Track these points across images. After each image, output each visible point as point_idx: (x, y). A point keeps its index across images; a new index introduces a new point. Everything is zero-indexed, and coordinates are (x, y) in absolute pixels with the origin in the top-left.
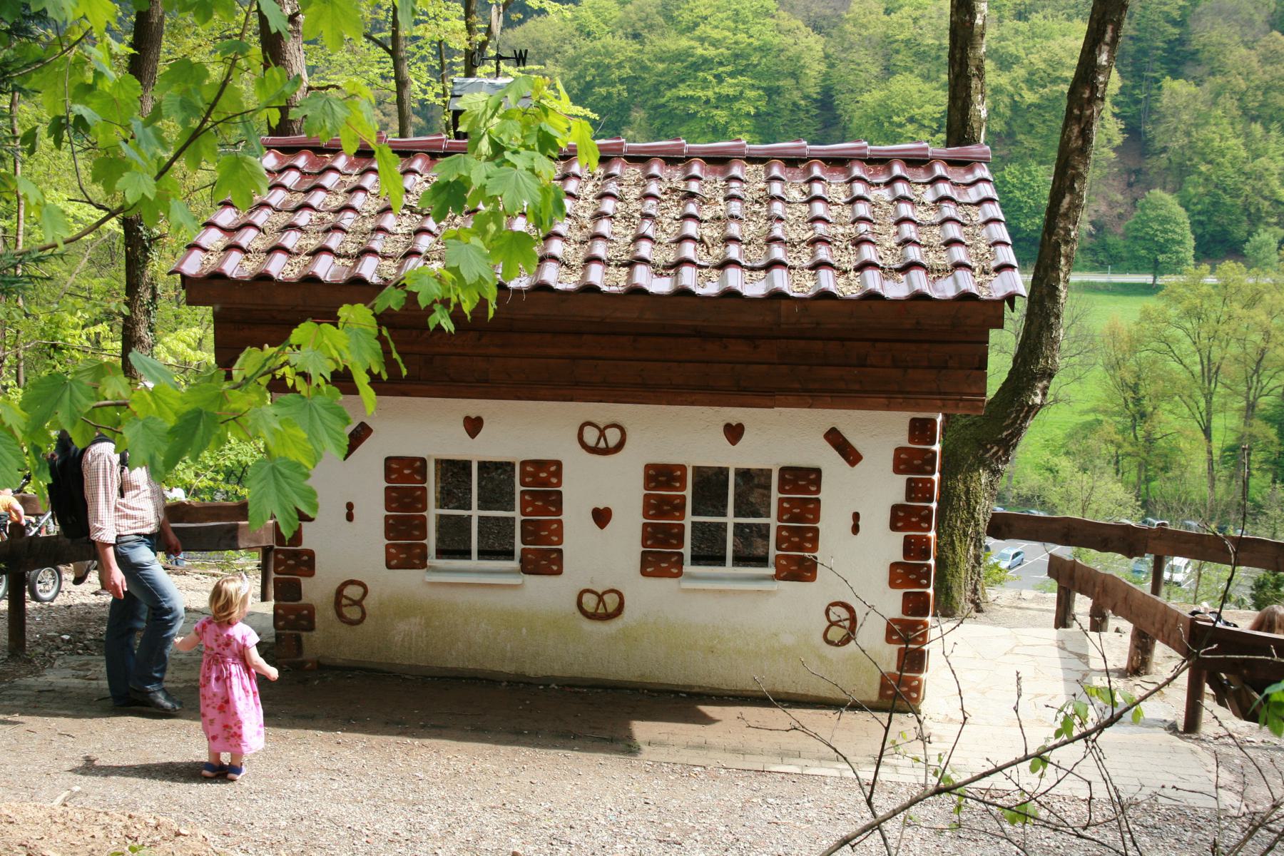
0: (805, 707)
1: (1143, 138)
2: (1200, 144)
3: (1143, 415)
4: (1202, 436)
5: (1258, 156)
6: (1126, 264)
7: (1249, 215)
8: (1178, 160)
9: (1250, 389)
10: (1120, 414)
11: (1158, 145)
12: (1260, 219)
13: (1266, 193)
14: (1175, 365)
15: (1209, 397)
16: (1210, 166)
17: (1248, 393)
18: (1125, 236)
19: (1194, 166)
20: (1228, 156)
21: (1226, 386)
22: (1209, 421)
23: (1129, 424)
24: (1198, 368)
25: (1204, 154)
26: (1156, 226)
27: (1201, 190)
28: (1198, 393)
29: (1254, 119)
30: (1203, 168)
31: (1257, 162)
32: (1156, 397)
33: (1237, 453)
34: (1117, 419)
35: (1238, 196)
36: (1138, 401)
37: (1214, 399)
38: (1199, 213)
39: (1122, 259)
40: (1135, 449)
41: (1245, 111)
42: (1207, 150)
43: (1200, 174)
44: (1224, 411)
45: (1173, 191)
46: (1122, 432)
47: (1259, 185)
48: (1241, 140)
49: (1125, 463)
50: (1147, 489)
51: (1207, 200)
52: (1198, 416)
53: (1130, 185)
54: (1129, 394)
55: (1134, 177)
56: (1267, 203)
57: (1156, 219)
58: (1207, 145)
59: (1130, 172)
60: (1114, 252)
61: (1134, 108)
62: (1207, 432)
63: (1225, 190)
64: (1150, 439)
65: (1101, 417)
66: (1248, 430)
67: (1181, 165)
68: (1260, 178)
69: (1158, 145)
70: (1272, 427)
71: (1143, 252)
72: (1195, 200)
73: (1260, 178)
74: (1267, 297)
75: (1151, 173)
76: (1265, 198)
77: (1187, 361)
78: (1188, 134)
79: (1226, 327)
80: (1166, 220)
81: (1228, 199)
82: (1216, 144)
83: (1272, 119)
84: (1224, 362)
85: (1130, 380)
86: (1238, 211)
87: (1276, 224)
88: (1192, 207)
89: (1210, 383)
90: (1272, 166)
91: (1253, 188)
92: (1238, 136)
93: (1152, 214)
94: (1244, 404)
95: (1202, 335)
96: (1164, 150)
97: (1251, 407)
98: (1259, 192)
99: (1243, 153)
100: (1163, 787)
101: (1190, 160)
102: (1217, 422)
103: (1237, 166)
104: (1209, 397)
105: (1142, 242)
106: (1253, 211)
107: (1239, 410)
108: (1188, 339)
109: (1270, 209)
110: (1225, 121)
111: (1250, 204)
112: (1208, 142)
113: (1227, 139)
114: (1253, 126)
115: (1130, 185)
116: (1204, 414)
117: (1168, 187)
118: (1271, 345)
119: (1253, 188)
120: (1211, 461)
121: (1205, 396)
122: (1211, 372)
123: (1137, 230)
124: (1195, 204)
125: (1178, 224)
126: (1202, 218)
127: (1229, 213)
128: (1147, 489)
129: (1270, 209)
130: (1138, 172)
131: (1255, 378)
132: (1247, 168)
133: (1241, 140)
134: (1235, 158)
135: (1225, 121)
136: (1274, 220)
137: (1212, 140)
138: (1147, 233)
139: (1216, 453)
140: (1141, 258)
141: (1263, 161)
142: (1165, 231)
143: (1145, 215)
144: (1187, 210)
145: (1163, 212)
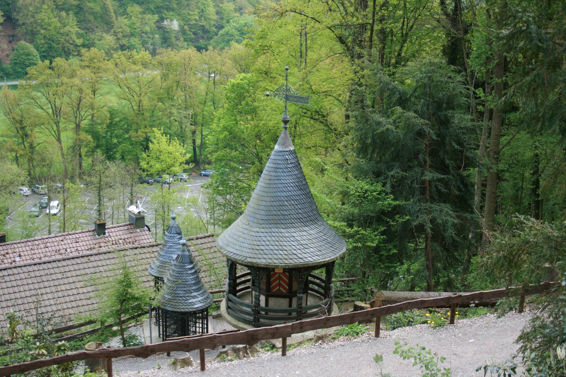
0: (276, 310)
1: (14, 21)
2: (39, 21)
3: (26, 135)
4: (57, 143)
5: (65, 26)
6: (12, 77)
7: (65, 52)
8: (31, 29)
9: (76, 117)
10: (15, 137)
11: (20, 22)
12: (70, 53)
13: (71, 42)
14: (39, 110)
15: (57, 124)
16: (45, 31)
17: (76, 120)
18: (10, 64)
19: (38, 31)
20: (53, 26)
21: (64, 118)
22: (59, 135)
23: (21, 141)
24: (50, 111)
25: (42, 26)
26: (24, 57)
27: (43, 41)
28: (52, 122)
29: (62, 9)
30: (42, 32)
31: (65, 29)
32: (32, 125)
33: (76, 148)
34: (14, 139)
35: (59, 44)
36: (23, 128)
37: (60, 124)
38: (43, 52)
39: (11, 75)
40: (25, 152)
41: (57, 7)
42: (43, 24)
43: (41, 34)
44: (66, 130)
45: (31, 43)
46: (19, 144)
47: (67, 38)
48: (57, 19)
49: (21, 160)
50: (34, 172)
51: (46, 46)
52: (53, 133)
53: (10, 42)
54: (18, 125)
55: (11, 38)
56: (72, 46)
57: (24, 54)
58: (42, 21)
59: (9, 36)
60: (7, 71)
61: (7, 7)
62: (59, 140)
63: (53, 41)
64: (32, 147)
65: (6, 139)
66: (78, 137)
67: (32, 31)
68: (67, 35)
69: (20, 22)
70: (89, 135)
71: (20, 70)
72: (41, 46)
73: (67, 35)
74: (78, 72)
75: (19, 35)
76: (71, 44)
77: (45, 107)
78: (33, 17)
79: (61, 88)
80: (28, 55)
81: (55, 45)
82: (47, 21)
83: (69, 10)
84: (63, 105)
85: (18, 118)
86: (60, 50)
87: (77, 55)
88: (40, 49)
89: (57, 117)
90: (72, 30)
91: (65, 40)
92: (55, 17)
93: (22, 52)
94: (74, 126)
95: (50, 93)
96: (24, 24)
97: (78, 126)
98: (68, 41)
99: (59, 25)
100: (424, 349)
101: (36, 28)
102: (63, 136)
103: (57, 30)
104: (57, 124)
105: (19, 65)
106: (66, 50)
107: (73, 129)
108: (44, 97)
109: (74, 49)
110: (49, 11)
111: (65, 47)
112: (43, 20)
113: (51, 18)
114: (61, 12)
115: (10, 42)
116: (56, 132)
117: (28, 40)
118: (83, 95)
119: (65, 40)
120: (63, 154)
121: (55, 123)
122: (57, 112)
123: (16, 59)
124: (41, 48)
125: (34, 56)
126: (44, 54)
127: (56, 51)
128: (34, 172)
129: (74, 49)
130: (13, 36)
131: (78, 112)
132: (61, 31)
133: (57, 19)
134: (55, 27)
135: (49, 11)
136: (76, 53)
137: (45, 19)
138: (21, 61)
139: (65, 151)
140: (19, 72)
141: (67, 28)
142: (29, 59)
143: (19, 52)
144: (38, 50)
145: (27, 51)
